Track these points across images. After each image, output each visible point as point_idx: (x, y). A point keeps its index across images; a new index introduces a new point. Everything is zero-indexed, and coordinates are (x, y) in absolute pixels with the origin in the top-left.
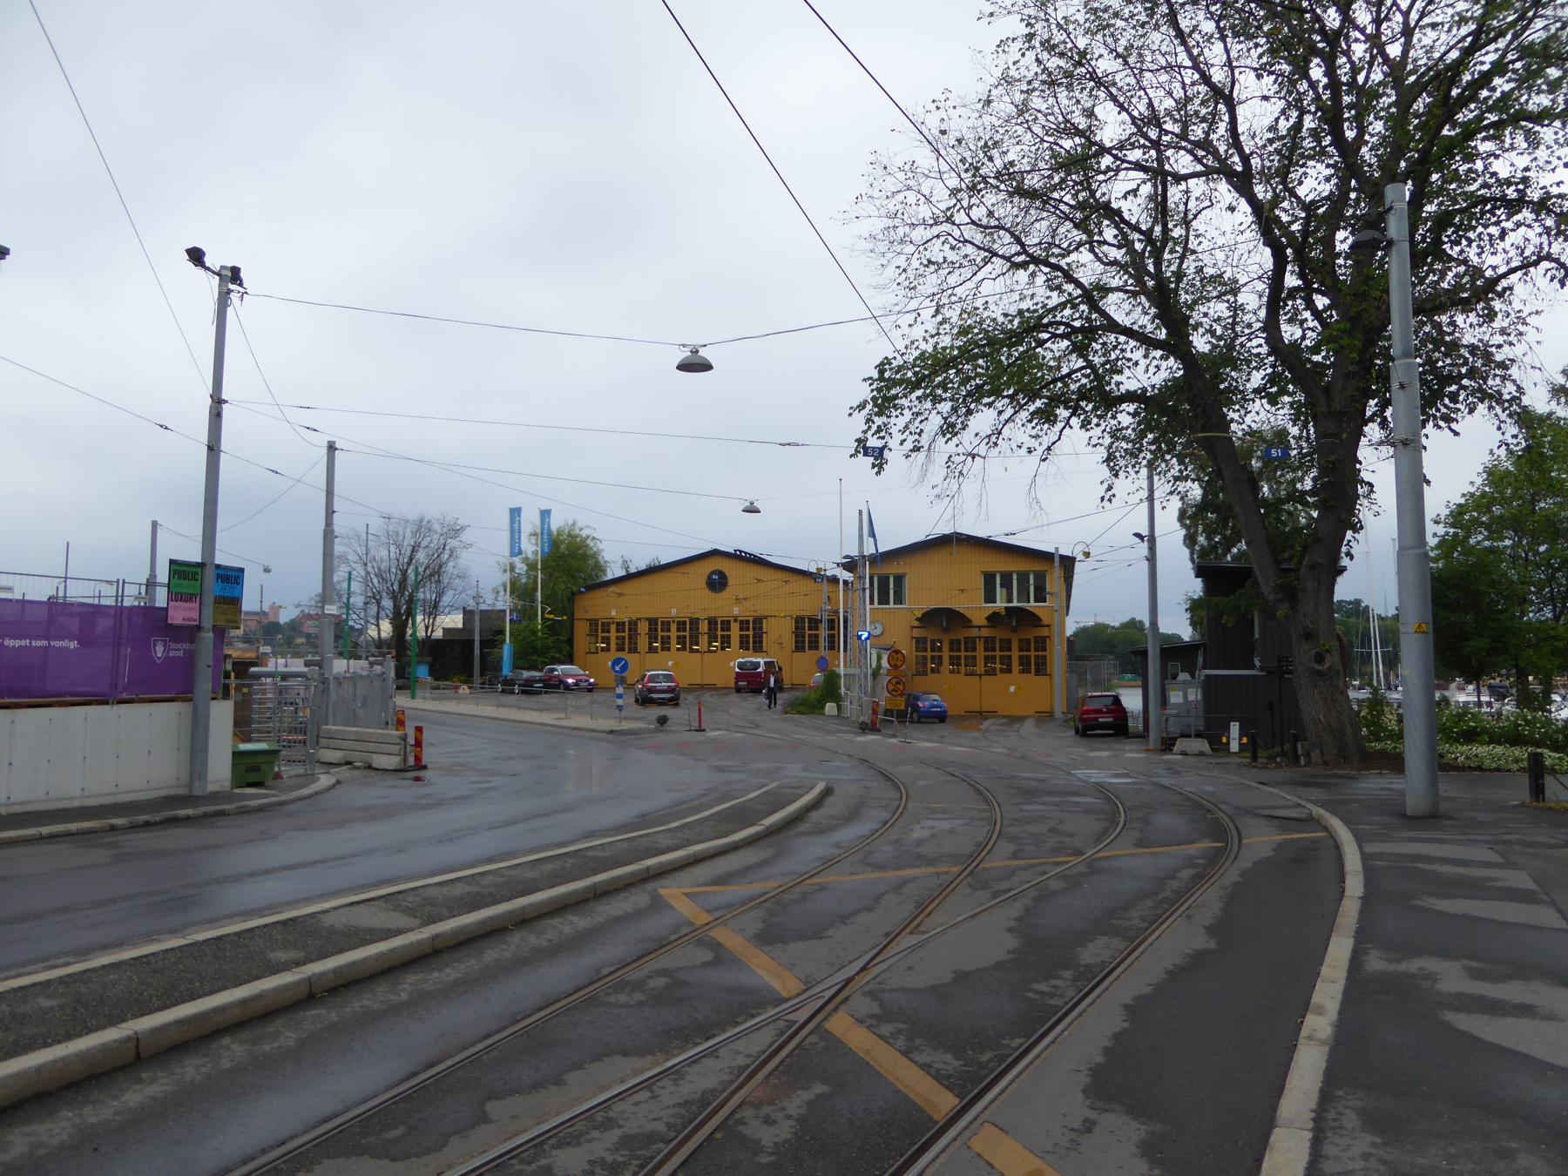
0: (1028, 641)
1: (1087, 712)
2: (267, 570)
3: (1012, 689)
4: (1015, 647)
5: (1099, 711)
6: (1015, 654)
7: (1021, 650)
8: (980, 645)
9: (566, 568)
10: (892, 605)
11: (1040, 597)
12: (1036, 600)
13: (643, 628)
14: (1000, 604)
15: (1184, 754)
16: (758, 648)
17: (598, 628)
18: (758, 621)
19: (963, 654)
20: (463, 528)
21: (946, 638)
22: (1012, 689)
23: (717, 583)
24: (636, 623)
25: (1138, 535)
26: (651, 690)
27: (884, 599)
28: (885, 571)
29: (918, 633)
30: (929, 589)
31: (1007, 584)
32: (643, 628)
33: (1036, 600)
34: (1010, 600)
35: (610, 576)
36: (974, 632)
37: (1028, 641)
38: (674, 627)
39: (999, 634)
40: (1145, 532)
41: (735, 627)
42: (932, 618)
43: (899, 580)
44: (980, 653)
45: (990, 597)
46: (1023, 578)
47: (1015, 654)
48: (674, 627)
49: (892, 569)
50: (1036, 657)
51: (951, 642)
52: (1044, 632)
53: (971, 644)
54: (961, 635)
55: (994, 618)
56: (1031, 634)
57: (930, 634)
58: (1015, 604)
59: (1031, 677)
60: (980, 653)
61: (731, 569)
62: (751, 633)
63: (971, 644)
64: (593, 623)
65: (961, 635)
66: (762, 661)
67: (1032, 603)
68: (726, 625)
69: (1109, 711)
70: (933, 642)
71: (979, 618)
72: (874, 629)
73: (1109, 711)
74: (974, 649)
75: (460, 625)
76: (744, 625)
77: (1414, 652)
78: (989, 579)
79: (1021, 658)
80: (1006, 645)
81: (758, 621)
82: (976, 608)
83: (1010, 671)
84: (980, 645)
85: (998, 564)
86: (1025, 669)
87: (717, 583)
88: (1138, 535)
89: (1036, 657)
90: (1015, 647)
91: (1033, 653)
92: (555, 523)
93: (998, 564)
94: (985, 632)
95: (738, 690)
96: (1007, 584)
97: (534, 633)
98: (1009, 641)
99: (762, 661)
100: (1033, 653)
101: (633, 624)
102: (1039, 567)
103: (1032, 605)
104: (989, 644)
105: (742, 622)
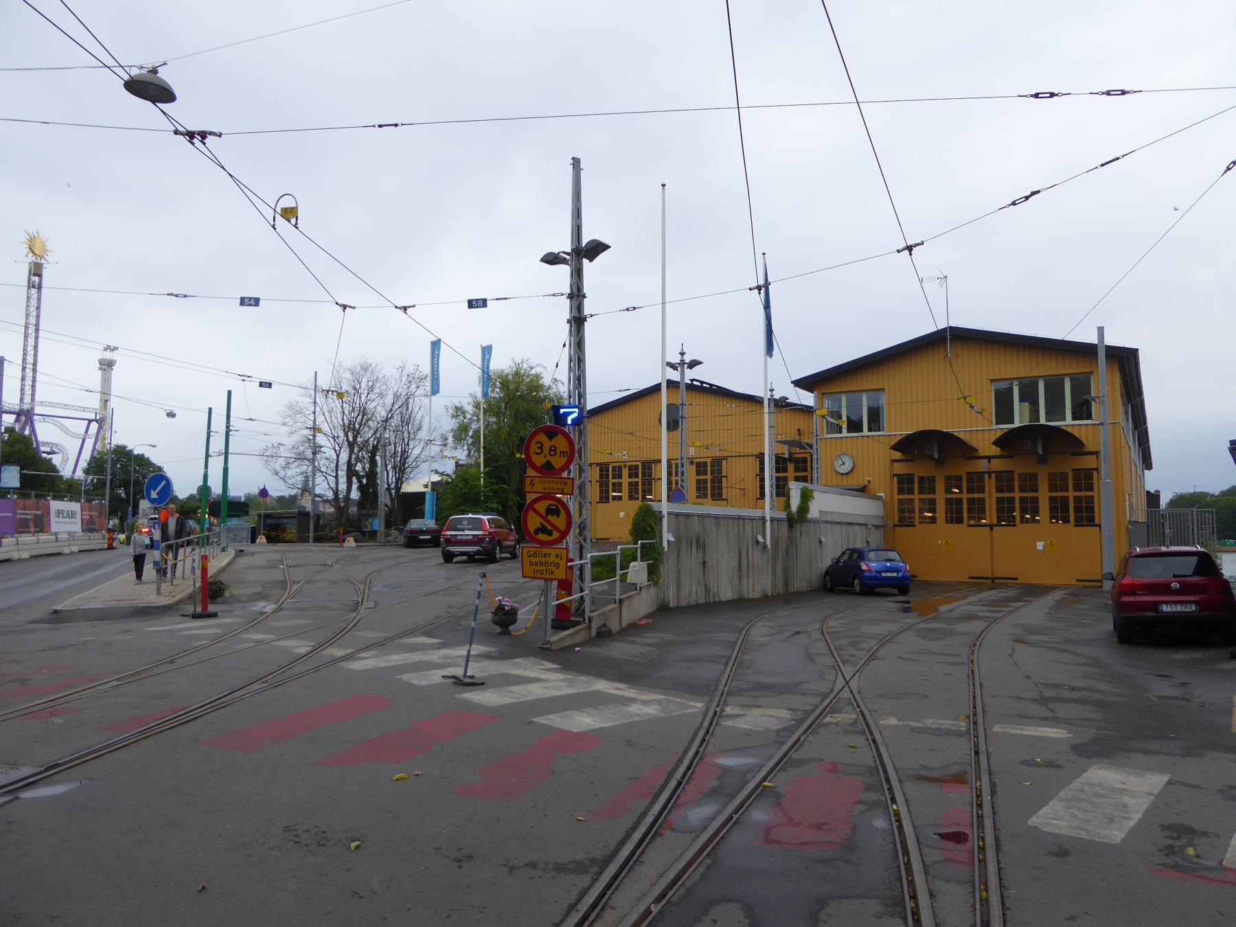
0: (1064, 476)
1: (1132, 589)
2: (171, 415)
3: (1040, 546)
4: (940, 486)
5: (1162, 588)
6: (1044, 496)
8: (990, 484)
10: (845, 433)
11: (1082, 410)
14: (1020, 419)
19: (1017, 495)
22: (1040, 546)
24: (720, 464)
29: (900, 469)
30: (914, 406)
31: (1029, 395)
36: (982, 466)
37: (1064, 476)
38: (625, 472)
39: (1019, 467)
42: (911, 446)
44: (990, 495)
47: (1044, 496)
48: (625, 472)
50: (911, 492)
51: (1052, 477)
52: (1089, 462)
53: (976, 482)
56: (1068, 466)
57: (918, 470)
59: (1069, 531)
62: (709, 477)
63: (976, 482)
67: (1069, 420)
69: (1186, 589)
70: (921, 480)
71: (986, 447)
73: (1186, 589)
74: (620, 477)
76: (633, 472)
77: (1102, 551)
79: (1052, 500)
80: (1030, 483)
81: (717, 462)
82: (979, 429)
84: (990, 484)
86: (1059, 511)
92: (501, 363)
93: (1018, 367)
94: (997, 465)
96: (1029, 395)
100: (1071, 494)
102: (1076, 367)
105: (698, 465)
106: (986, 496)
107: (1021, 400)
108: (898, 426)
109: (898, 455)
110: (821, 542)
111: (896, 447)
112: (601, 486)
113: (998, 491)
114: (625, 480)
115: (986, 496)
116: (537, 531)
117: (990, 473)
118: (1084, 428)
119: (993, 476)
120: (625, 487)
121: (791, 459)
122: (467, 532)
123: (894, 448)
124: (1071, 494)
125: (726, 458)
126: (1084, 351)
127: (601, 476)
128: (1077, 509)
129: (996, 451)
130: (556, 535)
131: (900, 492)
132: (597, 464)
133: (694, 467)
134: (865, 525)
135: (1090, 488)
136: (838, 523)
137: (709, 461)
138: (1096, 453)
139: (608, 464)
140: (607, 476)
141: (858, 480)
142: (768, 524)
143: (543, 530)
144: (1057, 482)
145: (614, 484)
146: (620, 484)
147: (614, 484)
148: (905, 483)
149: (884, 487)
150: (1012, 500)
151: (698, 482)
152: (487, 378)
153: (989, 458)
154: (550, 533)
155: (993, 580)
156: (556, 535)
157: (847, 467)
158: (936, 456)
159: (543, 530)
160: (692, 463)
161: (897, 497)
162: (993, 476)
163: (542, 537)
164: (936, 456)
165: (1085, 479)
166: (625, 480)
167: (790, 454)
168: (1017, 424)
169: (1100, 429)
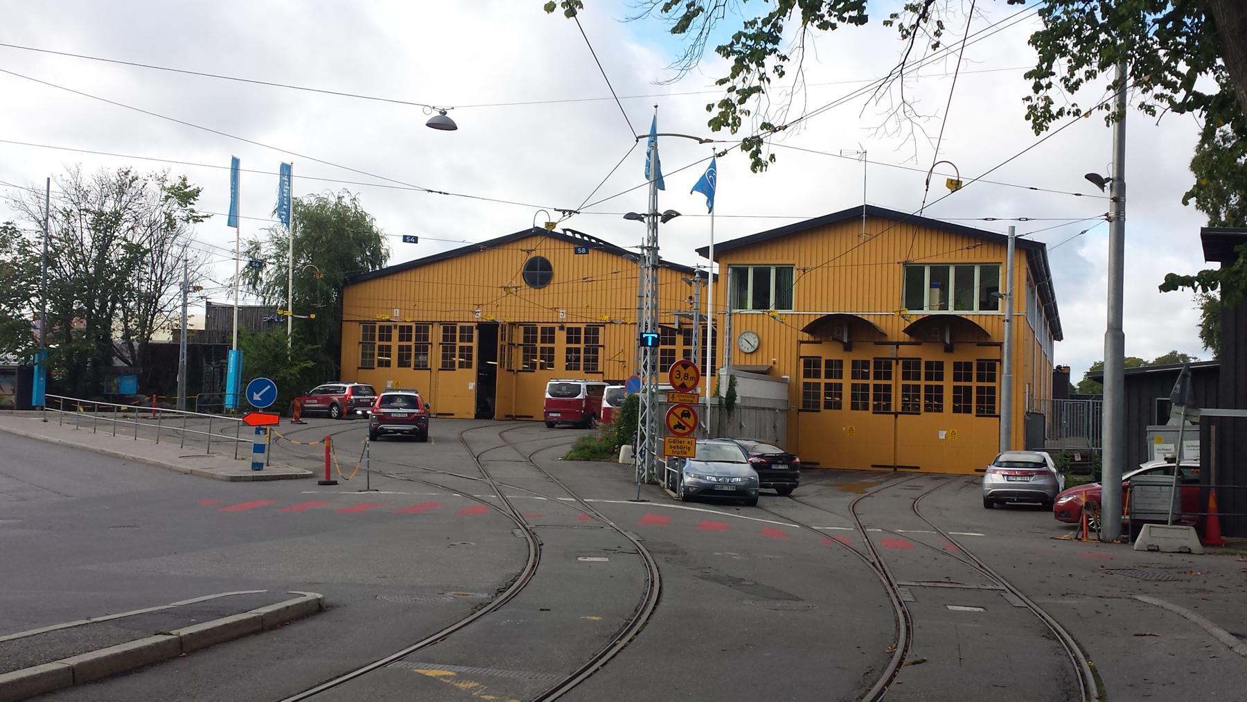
4: (948, 372)
7: (854, 376)
8: (897, 370)
9: (333, 248)
11: (989, 302)
12: (983, 306)
13: (436, 335)
15: (1154, 549)
16: (591, 368)
17: (376, 333)
18: (593, 331)
20: (78, 188)
21: (847, 360)
23: (538, 273)
24: (426, 329)
25: (1093, 178)
26: (383, 418)
27: (761, 302)
28: (757, 265)
30: (823, 288)
32: (436, 335)
33: (983, 306)
34: (944, 307)
35: (390, 263)
36: (887, 352)
38: (395, 334)
39: (926, 354)
40: (1107, 171)
41: (561, 336)
42: (822, 328)
43: (785, 273)
44: (897, 382)
45: (913, 298)
46: (964, 273)
47: (948, 384)
48: (395, 334)
49: (773, 258)
51: (957, 366)
52: (990, 353)
53: (883, 367)
54: (867, 354)
55: (922, 331)
56: (971, 355)
57: (826, 352)
58: (951, 311)
60: (897, 382)
61: (561, 259)
62: (582, 346)
63: (883, 367)
64: (368, 327)
65: (971, 355)
66: (583, 385)
68: (549, 335)
70: (929, 364)
72: (758, 348)
74: (888, 377)
75: (203, 328)
76: (573, 335)
78: (913, 275)
79: (956, 390)
80: (935, 370)
81: (593, 331)
82: (886, 309)
83: (939, 409)
84: (897, 370)
85: (929, 251)
86: (962, 403)
87: (538, 273)
88: (1093, 178)
89: (980, 390)
90: (948, 372)
91: (974, 384)
92: (305, 191)
93: (929, 251)
94: (907, 352)
95: (551, 425)
97: (280, 343)
98: (940, 365)
99: (583, 385)
101: (423, 328)
102: (979, 256)
103: (974, 313)
104: (911, 368)
105: (570, 331)
106: (901, 382)
107: (932, 286)
108: (812, 301)
109: (806, 336)
110: (741, 427)
111: (810, 329)
112: (445, 349)
113: (904, 379)
114: (395, 343)
115: (901, 382)
116: (675, 427)
117: (897, 360)
118: (989, 319)
119: (900, 362)
120: (395, 352)
121: (680, 331)
122: (402, 410)
123: (805, 330)
124: (974, 384)
125: (603, 325)
126: (997, 241)
127: (445, 338)
128: (979, 400)
129: (907, 337)
130: (687, 429)
131: (807, 374)
132: (440, 323)
133: (564, 334)
134: (773, 409)
135: (992, 378)
136: (755, 408)
137: (583, 326)
138: (1000, 345)
139: (455, 323)
140: (454, 338)
141: (761, 361)
142: (708, 411)
143: (679, 426)
144: (962, 371)
145: (381, 347)
146: (389, 348)
147: (381, 347)
148: (811, 365)
149: (790, 369)
150: (866, 387)
151: (569, 351)
152: (286, 207)
153: (898, 344)
154: (684, 428)
155: (895, 468)
156: (687, 429)
157: (755, 343)
158: (845, 340)
159: (679, 426)
160: (562, 328)
161: (803, 380)
162: (900, 362)
163: (679, 430)
164: (845, 340)
165: (988, 369)
166: (395, 343)
167: (680, 324)
168: (926, 312)
169: (1007, 318)
